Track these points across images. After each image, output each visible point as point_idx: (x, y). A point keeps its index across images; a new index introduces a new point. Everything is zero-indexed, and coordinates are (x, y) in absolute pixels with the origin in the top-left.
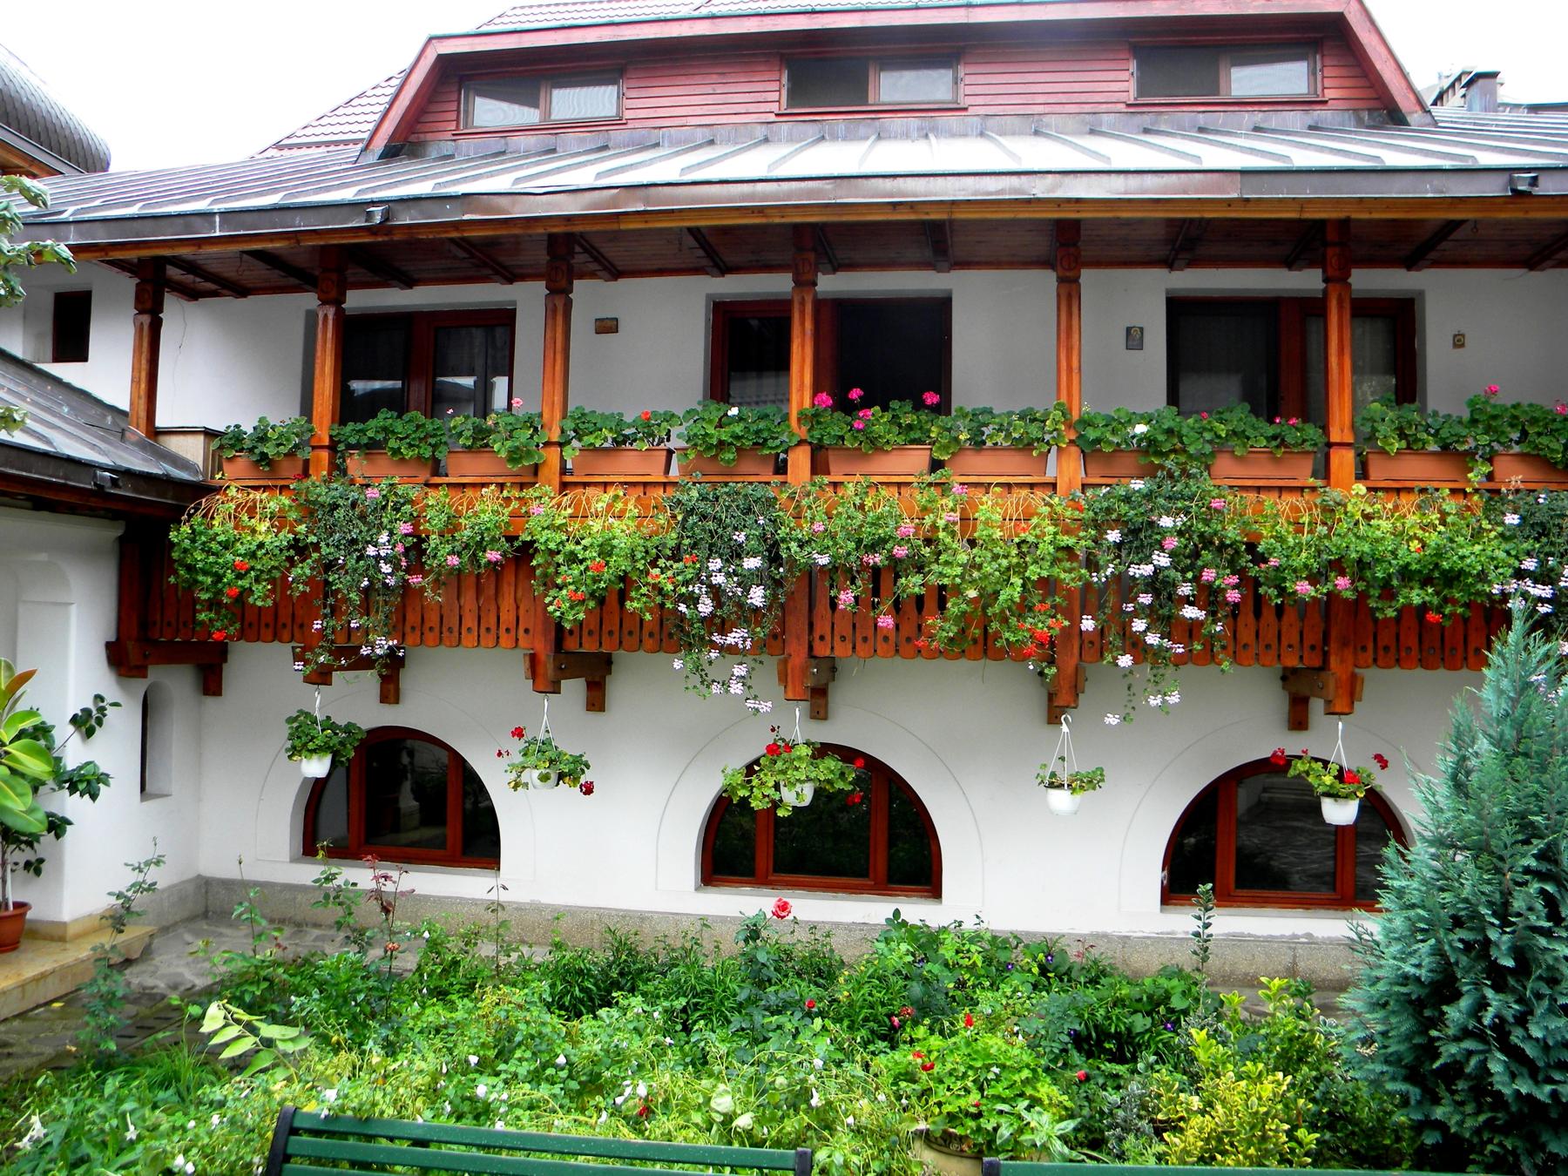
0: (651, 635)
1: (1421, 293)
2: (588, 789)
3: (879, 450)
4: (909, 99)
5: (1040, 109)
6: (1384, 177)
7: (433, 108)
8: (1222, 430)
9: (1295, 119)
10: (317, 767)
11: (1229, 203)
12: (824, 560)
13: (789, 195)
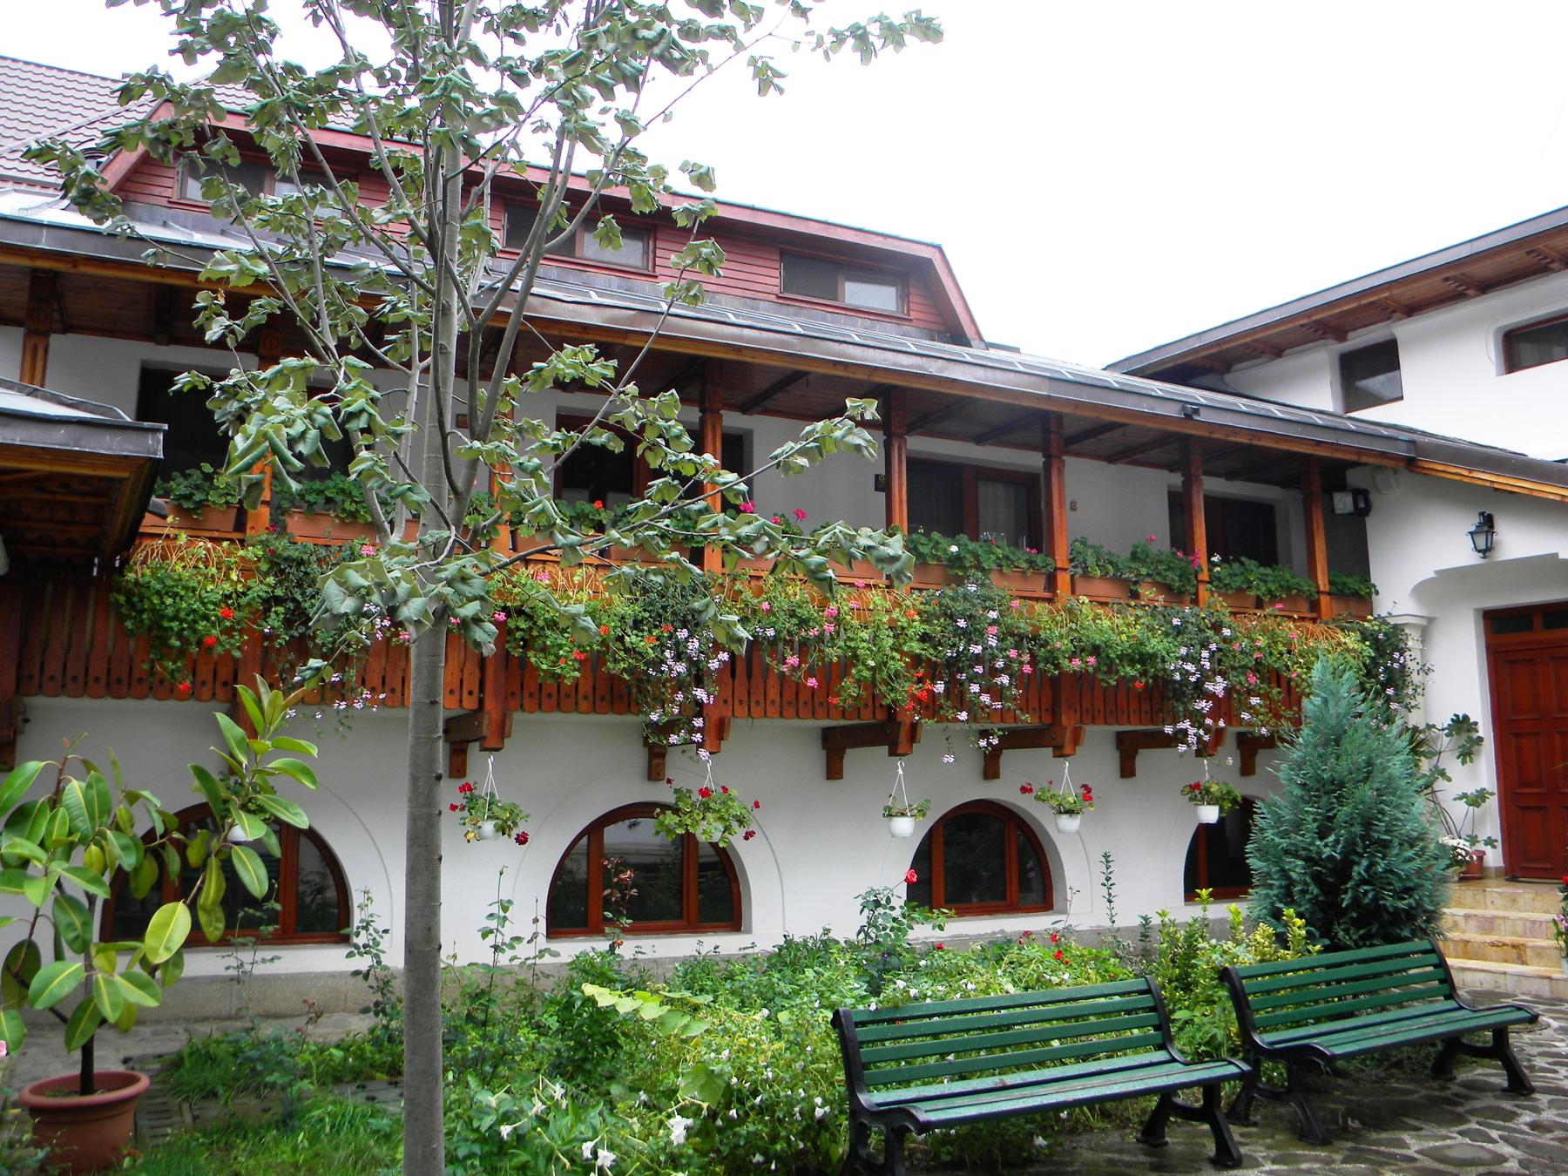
0: (585, 697)
1: (750, 433)
2: (522, 839)
4: (623, 261)
5: (719, 289)
7: (144, 179)
8: (1144, 571)
10: (1210, 814)
11: (1039, 397)
12: (771, 633)
13: (768, 342)
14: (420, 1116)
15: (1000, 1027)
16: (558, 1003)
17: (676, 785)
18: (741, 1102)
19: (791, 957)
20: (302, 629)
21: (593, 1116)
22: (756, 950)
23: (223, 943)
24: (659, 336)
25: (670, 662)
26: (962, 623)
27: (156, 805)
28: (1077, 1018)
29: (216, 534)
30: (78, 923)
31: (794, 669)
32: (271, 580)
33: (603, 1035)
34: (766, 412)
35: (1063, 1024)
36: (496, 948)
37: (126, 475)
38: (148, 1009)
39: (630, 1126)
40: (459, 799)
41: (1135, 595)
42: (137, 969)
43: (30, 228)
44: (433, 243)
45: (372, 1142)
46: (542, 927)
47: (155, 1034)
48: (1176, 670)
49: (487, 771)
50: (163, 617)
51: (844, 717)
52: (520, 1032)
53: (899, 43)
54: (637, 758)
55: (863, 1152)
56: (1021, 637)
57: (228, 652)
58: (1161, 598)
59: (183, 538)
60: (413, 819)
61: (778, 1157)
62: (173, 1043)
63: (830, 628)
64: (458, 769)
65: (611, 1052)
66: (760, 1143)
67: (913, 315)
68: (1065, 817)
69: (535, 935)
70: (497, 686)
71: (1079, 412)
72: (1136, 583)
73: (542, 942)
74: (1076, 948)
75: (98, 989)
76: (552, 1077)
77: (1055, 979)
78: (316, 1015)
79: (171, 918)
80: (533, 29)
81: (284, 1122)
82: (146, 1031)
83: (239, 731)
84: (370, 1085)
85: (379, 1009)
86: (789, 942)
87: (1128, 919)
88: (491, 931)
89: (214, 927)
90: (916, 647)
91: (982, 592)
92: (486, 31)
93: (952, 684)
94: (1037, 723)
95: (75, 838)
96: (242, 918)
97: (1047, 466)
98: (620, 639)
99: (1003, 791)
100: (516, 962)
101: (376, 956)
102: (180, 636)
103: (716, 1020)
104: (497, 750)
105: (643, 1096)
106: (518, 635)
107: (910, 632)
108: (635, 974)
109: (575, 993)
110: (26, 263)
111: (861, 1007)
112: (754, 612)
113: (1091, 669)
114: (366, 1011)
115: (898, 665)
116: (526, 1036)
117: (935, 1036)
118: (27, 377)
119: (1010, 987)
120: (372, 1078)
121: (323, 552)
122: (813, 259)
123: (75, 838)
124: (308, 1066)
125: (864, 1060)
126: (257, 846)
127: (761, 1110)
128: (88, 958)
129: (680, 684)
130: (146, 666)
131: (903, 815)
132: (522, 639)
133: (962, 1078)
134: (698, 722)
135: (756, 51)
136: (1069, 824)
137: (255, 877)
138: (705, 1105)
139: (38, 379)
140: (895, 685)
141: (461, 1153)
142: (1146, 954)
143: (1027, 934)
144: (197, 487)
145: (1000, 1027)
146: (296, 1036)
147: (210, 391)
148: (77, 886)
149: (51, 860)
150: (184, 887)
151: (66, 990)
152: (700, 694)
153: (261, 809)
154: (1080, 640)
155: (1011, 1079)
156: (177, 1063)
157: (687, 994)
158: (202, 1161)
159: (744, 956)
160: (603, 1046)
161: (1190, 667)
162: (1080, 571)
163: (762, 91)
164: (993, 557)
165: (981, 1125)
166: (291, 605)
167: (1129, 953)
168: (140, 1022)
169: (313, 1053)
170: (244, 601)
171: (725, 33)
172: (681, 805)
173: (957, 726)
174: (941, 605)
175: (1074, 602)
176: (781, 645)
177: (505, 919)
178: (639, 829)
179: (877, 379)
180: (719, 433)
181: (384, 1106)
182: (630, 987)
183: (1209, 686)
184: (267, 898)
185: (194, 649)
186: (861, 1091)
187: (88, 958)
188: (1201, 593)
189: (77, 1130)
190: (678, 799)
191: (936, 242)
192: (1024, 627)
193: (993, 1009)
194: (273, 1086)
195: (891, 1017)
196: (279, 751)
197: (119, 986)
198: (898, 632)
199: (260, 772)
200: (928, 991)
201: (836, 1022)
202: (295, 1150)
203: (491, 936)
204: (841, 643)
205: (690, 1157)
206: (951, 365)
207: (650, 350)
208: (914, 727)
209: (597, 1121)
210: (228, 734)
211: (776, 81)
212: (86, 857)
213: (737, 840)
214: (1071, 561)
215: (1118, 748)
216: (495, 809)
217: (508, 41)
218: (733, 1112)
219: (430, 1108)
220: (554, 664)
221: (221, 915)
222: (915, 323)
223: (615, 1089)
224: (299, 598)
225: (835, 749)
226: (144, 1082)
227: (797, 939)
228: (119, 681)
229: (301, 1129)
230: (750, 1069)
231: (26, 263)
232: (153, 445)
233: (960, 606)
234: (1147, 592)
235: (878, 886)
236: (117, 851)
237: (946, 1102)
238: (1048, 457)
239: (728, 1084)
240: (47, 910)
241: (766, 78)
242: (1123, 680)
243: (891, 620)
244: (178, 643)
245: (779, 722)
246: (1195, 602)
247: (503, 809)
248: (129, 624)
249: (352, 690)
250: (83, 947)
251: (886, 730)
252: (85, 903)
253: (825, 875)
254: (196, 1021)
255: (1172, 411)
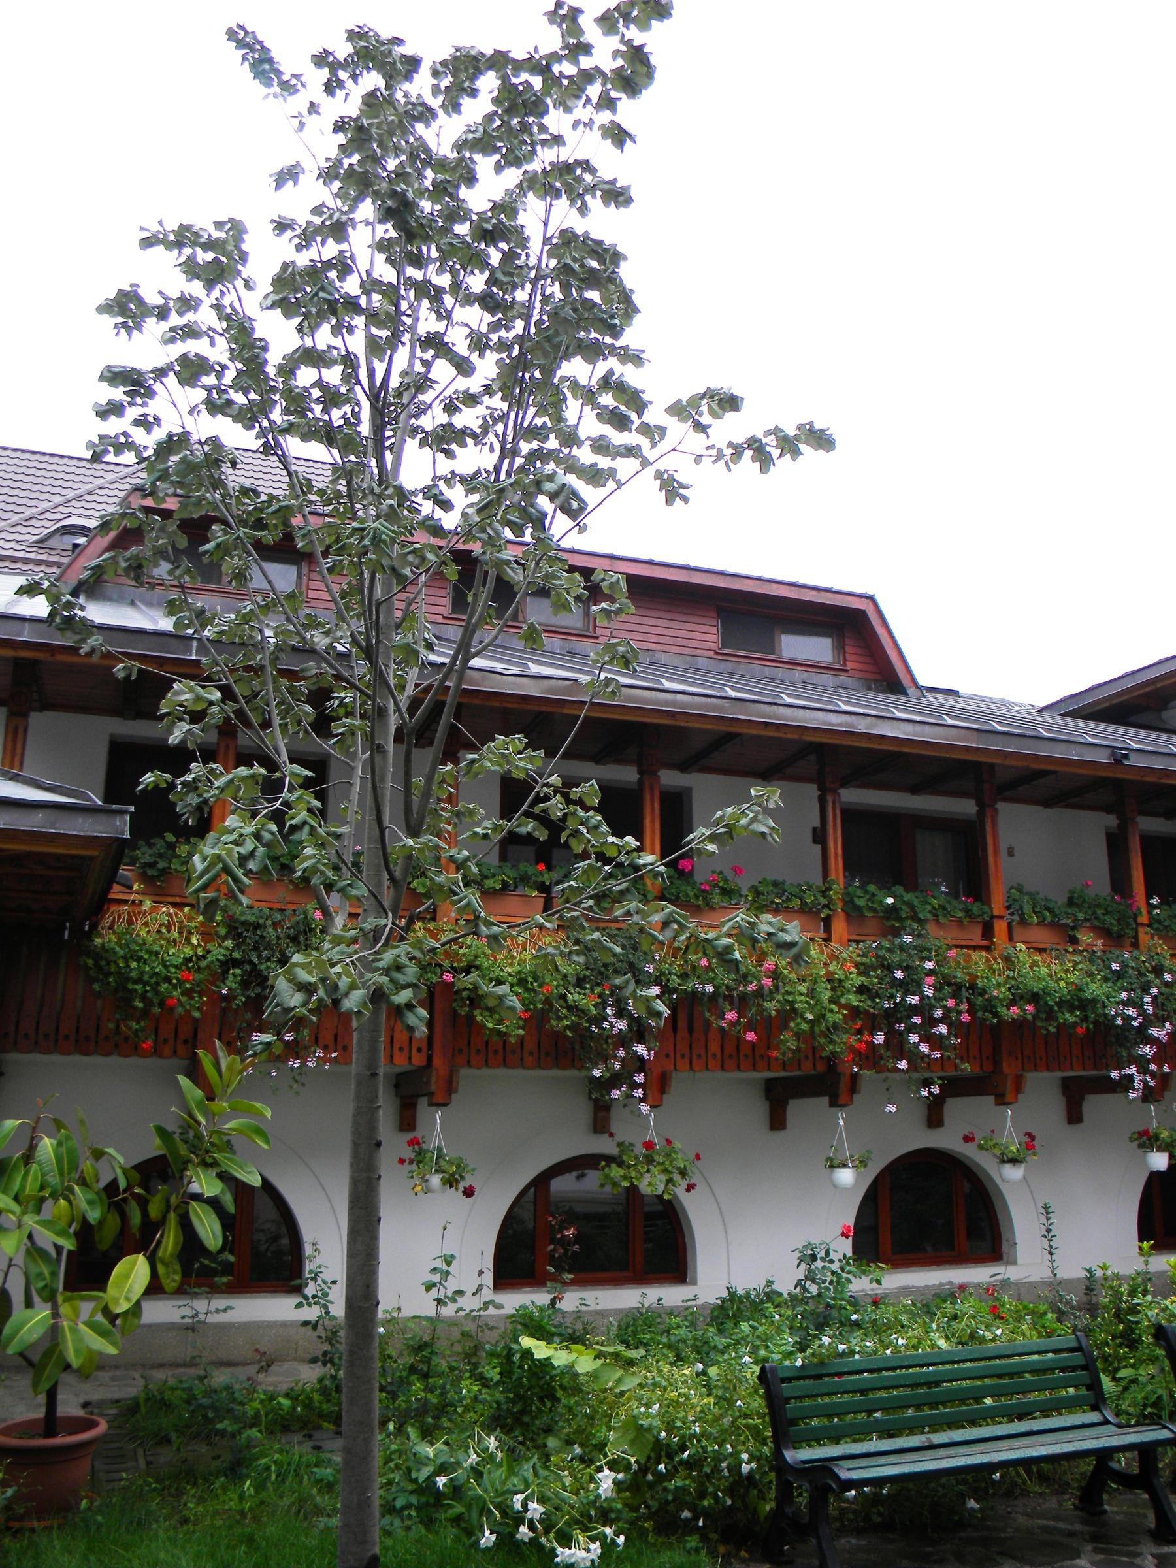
0: (531, 1053)
1: (689, 790)
2: (469, 1192)
3: (712, 908)
5: (659, 647)
6: (1036, 741)
8: (1081, 916)
9: (826, 679)
10: (1159, 1161)
12: (709, 988)
14: (357, 1463)
15: (929, 1384)
16: (498, 1356)
17: (619, 1138)
18: (670, 1456)
19: (733, 1309)
20: (258, 990)
21: (527, 1469)
22: (699, 1302)
23: (180, 1291)
24: (593, 704)
25: (612, 1019)
26: (899, 975)
27: (119, 1161)
28: (1011, 1375)
29: (178, 900)
30: (46, 1273)
31: (732, 1024)
32: (229, 943)
33: (541, 1388)
34: (703, 770)
35: (996, 1381)
36: (439, 1301)
37: (96, 853)
38: (109, 1356)
39: (561, 1479)
40: (408, 1153)
41: (1074, 941)
42: (100, 1318)
43: (11, 623)
44: (369, 653)
45: (314, 1491)
46: (488, 1279)
47: (113, 1379)
48: (1117, 1015)
49: (436, 1126)
50: (128, 979)
51: (784, 1069)
52: (464, 1384)
53: (796, 453)
54: (583, 1112)
55: (789, 1510)
56: (959, 986)
57: (188, 1012)
58: (1100, 942)
59: (147, 904)
60: (355, 1183)
61: (706, 1513)
62: (131, 1390)
63: (768, 983)
64: (407, 1122)
65: (549, 1404)
66: (688, 1498)
67: (849, 665)
68: (1008, 1166)
69: (480, 1288)
70: (434, 1052)
71: (1008, 762)
72: (1073, 928)
73: (488, 1294)
74: (1009, 1303)
75: (64, 1336)
76: (489, 1429)
77: (989, 1335)
78: (267, 1363)
79: (132, 1269)
80: (463, 444)
81: (232, 1470)
82: (104, 1376)
83: (199, 1093)
84: (317, 1435)
85: (326, 1359)
86: (732, 1295)
87: (1071, 1269)
88: (434, 1285)
89: (172, 1279)
90: (853, 999)
91: (918, 942)
92: (421, 446)
93: (891, 1034)
94: (977, 1071)
95: (46, 1193)
96: (196, 1271)
97: (981, 814)
98: (563, 997)
99: (947, 1139)
100: (461, 1313)
101: (325, 1307)
102: (143, 998)
103: (649, 1374)
104: (445, 1105)
105: (577, 1450)
106: (465, 994)
107: (848, 984)
108: (579, 1326)
109: (514, 1346)
110: (10, 653)
111: (787, 1363)
112: (694, 968)
113: (1029, 1017)
114: (314, 1360)
115: (836, 1017)
116: (468, 1388)
117: (863, 1392)
118: (7, 762)
119: (942, 1343)
120: (319, 1428)
121: (278, 916)
122: (750, 614)
123: (46, 1193)
124: (257, 1415)
125: (789, 1416)
126: (214, 1203)
127: (689, 1465)
128: (55, 1307)
129: (623, 1040)
130: (111, 1026)
131: (845, 1166)
132: (469, 998)
133: (891, 1436)
134: (640, 1078)
135: (661, 465)
136: (1013, 1173)
137: (209, 1230)
138: (633, 1460)
139: (17, 764)
140: (834, 1037)
141: (399, 1503)
142: (1092, 1309)
143: (962, 1287)
144: (161, 856)
145: (929, 1384)
146: (246, 1385)
147: (172, 786)
148: (47, 1238)
149: (24, 1213)
150: (143, 1240)
151: (36, 1336)
152: (641, 1050)
153: (215, 1164)
154: (1018, 988)
155: (938, 1438)
156: (131, 1409)
157: (621, 1348)
158: (153, 1505)
159: (687, 1308)
160: (541, 1399)
161: (1131, 1012)
162: (1016, 917)
163: (669, 501)
164: (929, 908)
165: (911, 1486)
166: (248, 967)
167: (1073, 1308)
168: (101, 1368)
169: (262, 1402)
170: (203, 964)
171: (630, 451)
172: (625, 1158)
173: (897, 1076)
174: (878, 957)
175: (1011, 951)
176: (721, 1000)
177: (448, 1273)
178: (586, 1180)
179: (809, 738)
180: (657, 793)
181: (328, 1455)
182: (574, 1339)
183: (1154, 1032)
184: (222, 1250)
185: (156, 1010)
186: (787, 1448)
187: (55, 1307)
188: (1141, 936)
189: (44, 1472)
190: (622, 1152)
191: (870, 592)
192: (960, 976)
193: (921, 1366)
194: (223, 1433)
195: (816, 1372)
196: (235, 1112)
197: (84, 1337)
198: (836, 985)
199: (217, 1132)
200: (861, 1345)
201: (763, 1377)
202: (241, 1497)
203: (435, 1290)
204: (779, 997)
205: (619, 1511)
206: (880, 722)
207: (586, 717)
208: (854, 1077)
209: (529, 1475)
210: (188, 1096)
211: (682, 491)
212: (56, 1211)
213: (680, 1191)
214: (1008, 908)
215: (1064, 1094)
216: (442, 1163)
217: (440, 456)
218: (662, 1467)
219: (366, 1457)
220: (500, 1022)
221: (178, 1267)
222: (851, 673)
223: (552, 1442)
224: (256, 960)
225: (778, 1101)
226: (103, 1427)
227: (740, 1292)
228: (87, 1039)
229: (248, 1476)
230: (679, 1424)
231: (10, 653)
232: (121, 826)
233: (896, 957)
234: (1085, 937)
235: (815, 1241)
236: (84, 1205)
237: (871, 1461)
238: (981, 805)
239: (657, 1440)
240: (20, 1260)
241: (672, 489)
242: (1062, 1027)
243: (828, 973)
244: (141, 1005)
245: (720, 1074)
246: (1135, 945)
247: (451, 1163)
248: (96, 987)
249: (306, 1048)
250: (50, 1297)
251: (828, 1082)
252: (53, 1253)
253: (769, 1229)
254: (153, 1367)
255: (1102, 757)
